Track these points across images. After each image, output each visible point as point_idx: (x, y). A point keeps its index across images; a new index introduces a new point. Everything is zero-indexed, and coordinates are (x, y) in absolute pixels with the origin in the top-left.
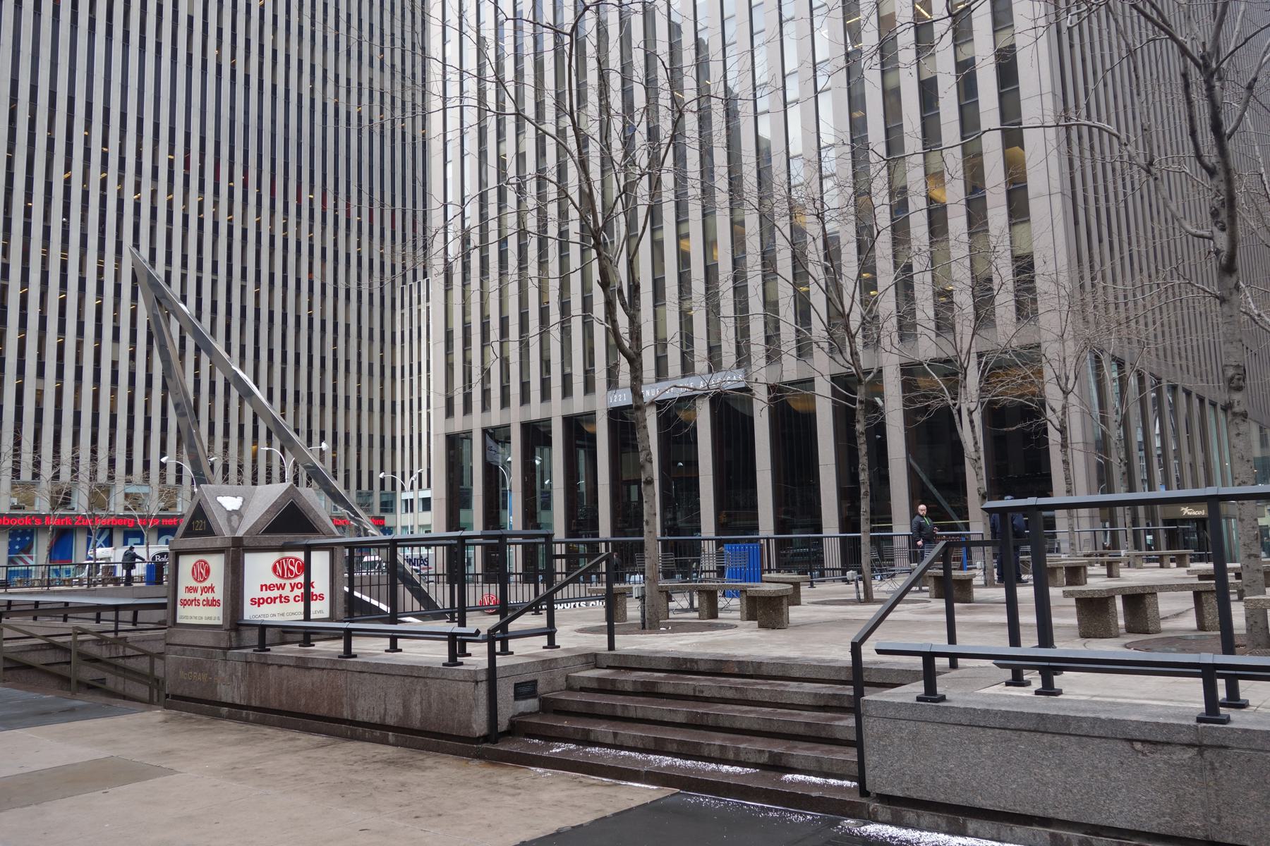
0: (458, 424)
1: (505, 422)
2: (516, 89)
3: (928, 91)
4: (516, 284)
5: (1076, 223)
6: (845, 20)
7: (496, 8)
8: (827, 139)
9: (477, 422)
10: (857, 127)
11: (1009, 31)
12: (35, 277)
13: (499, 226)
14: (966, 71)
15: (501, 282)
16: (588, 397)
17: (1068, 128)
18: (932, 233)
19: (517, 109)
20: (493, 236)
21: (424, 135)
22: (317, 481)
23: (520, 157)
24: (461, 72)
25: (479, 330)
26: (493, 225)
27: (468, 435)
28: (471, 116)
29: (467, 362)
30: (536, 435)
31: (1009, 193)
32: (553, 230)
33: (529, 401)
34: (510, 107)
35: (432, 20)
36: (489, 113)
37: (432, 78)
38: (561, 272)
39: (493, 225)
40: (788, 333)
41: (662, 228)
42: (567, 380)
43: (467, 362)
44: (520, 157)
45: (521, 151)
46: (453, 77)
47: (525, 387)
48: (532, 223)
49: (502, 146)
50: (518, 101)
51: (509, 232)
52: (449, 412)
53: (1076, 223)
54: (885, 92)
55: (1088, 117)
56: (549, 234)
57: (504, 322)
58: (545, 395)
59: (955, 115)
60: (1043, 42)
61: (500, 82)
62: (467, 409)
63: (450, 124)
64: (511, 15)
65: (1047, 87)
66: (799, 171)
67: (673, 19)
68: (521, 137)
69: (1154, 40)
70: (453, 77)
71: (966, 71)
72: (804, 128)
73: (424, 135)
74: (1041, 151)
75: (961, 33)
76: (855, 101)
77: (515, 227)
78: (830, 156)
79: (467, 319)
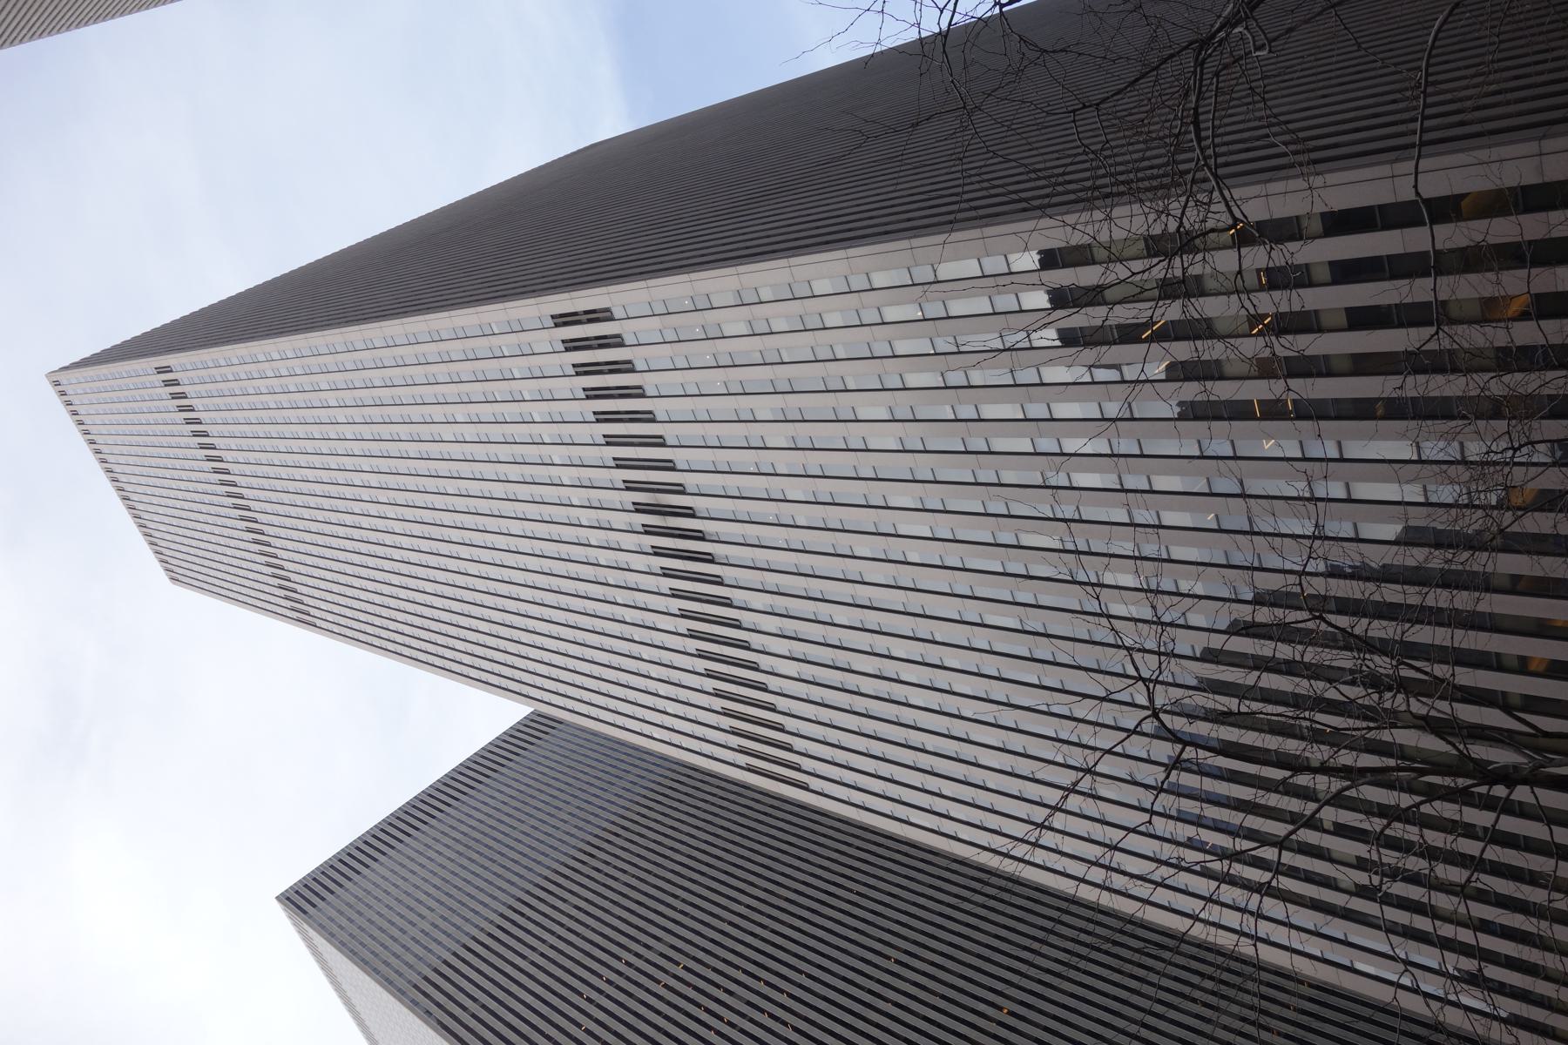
2: (1245, 837)
3: (1361, 319)
4: (1556, 927)
5: (997, 215)
6: (1254, 418)
7: (1134, 831)
8: (1407, 453)
10: (1395, 410)
11: (1305, 223)
12: (642, 1010)
13: (1451, 921)
14: (1346, 272)
15: (1551, 950)
17: (1422, 144)
19: (1273, 844)
20: (1465, 936)
21: (1310, 985)
24: (1209, 900)
26: (1447, 930)
28: (1273, 907)
31: (1528, 209)
32: (1470, 847)
34: (1269, 853)
35: (1139, 915)
36: (1274, 883)
37: (1211, 939)
38: (1549, 854)
39: (1447, 930)
41: (1503, 693)
46: (1214, 913)
48: (1455, 874)
49: (1342, 885)
50: (1263, 839)
51: (1462, 909)
53: (997, 215)
55: (1414, 120)
56: (1477, 854)
60: (1332, 178)
61: (1236, 856)
63: (1293, 942)
64: (1146, 817)
65: (1385, 170)
66: (1446, 494)
67: (1223, 627)
68: (1334, 855)
69: (1359, 45)
70: (1214, 913)
71: (1346, 272)
72: (1383, 480)
73: (1310, 985)
74: (1446, 175)
75: (1299, 277)
76: (1361, 410)
77: (1455, 900)
78: (1432, 450)
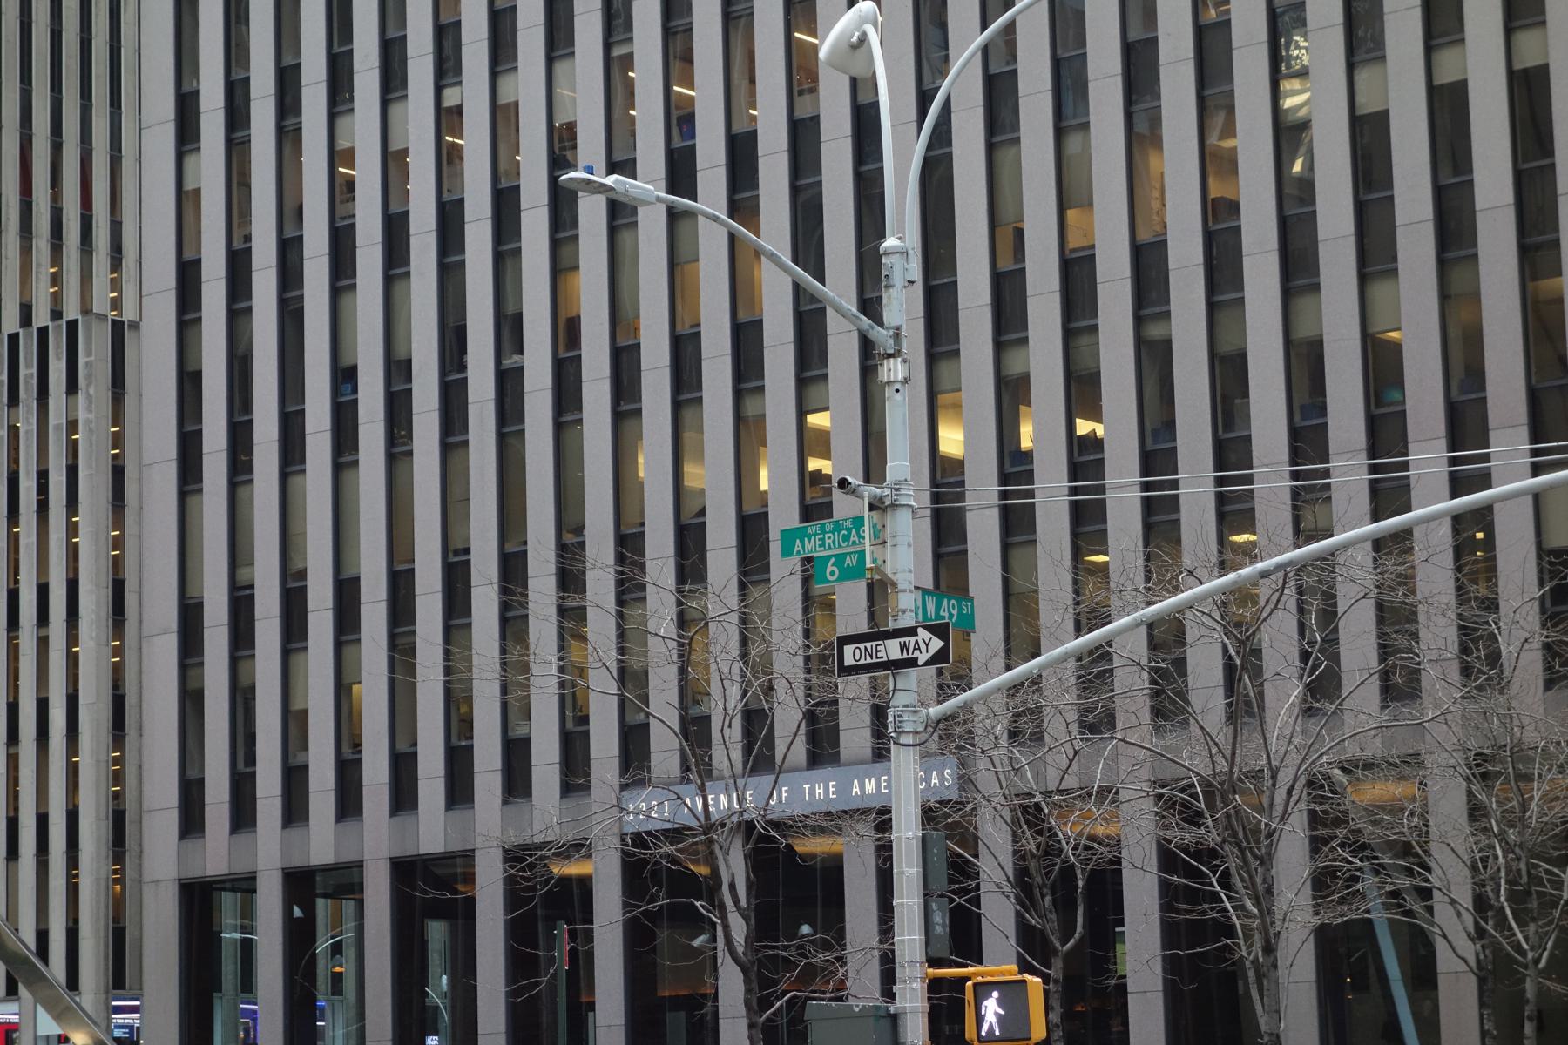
0: (216, 854)
1: (349, 856)
9: (268, 851)
14: (1448, 107)
16: (456, 814)
18: (682, 578)
22: (28, 985)
23: (393, 162)
25: (382, 591)
27: (344, 881)
29: (242, 698)
30: (430, 888)
33: (527, 792)
40: (1438, 634)
42: (403, 767)
43: (242, 698)
44: (393, 162)
45: (394, 146)
47: (295, 778)
52: (191, 821)
54: (1433, 91)
57: (347, 593)
58: (459, 790)
59: (1426, 210)
62: (243, 815)
71: (1448, 107)
79: (243, 575)
